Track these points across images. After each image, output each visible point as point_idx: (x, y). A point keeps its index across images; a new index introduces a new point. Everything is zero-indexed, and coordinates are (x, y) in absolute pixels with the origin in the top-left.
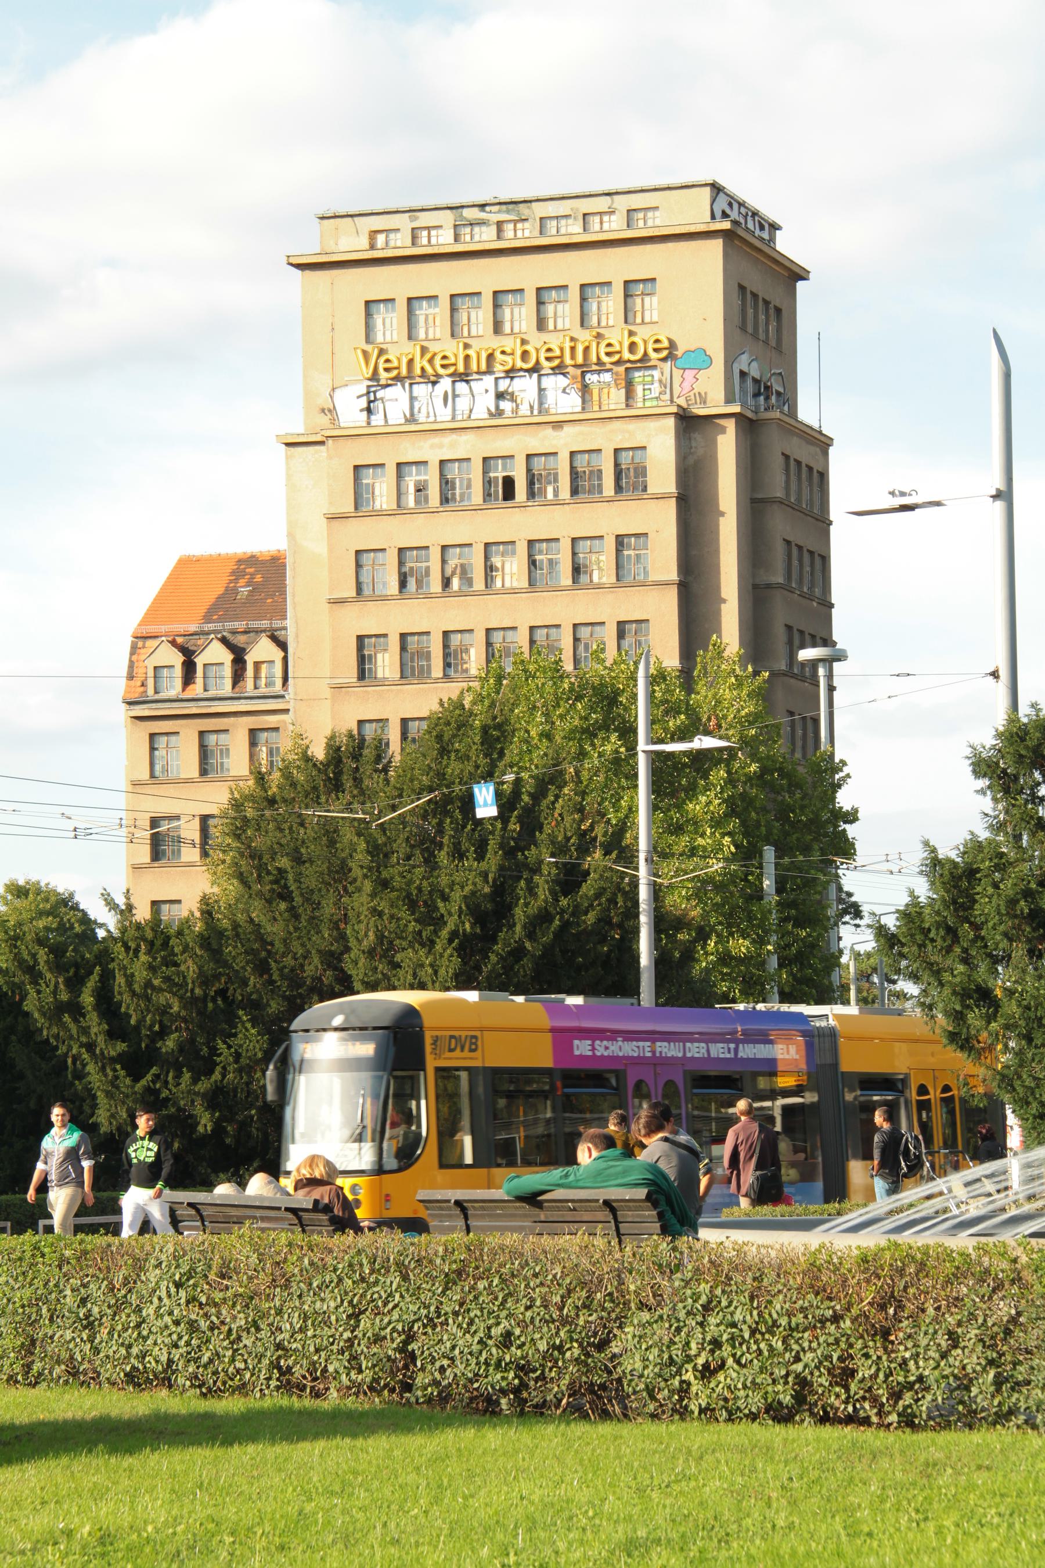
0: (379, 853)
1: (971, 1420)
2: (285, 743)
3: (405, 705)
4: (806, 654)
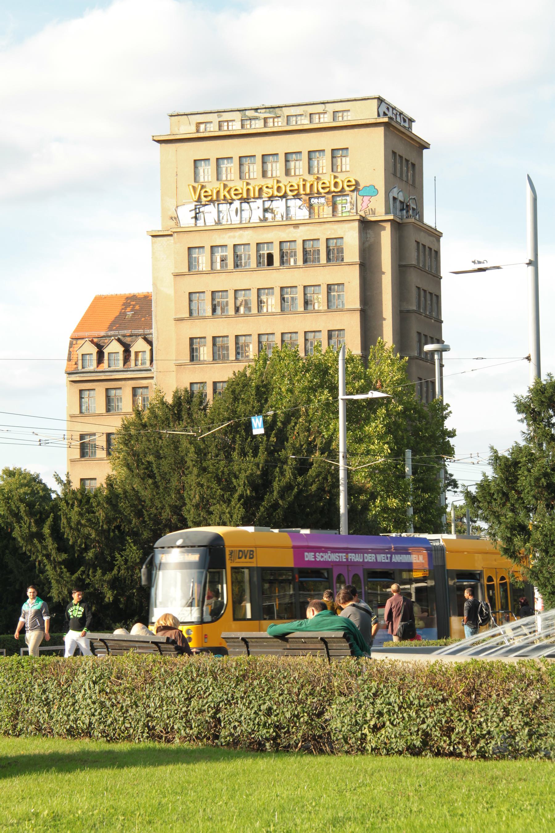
0: (201, 453)
1: (516, 754)
2: (151, 395)
3: (215, 374)
4: (428, 347)
